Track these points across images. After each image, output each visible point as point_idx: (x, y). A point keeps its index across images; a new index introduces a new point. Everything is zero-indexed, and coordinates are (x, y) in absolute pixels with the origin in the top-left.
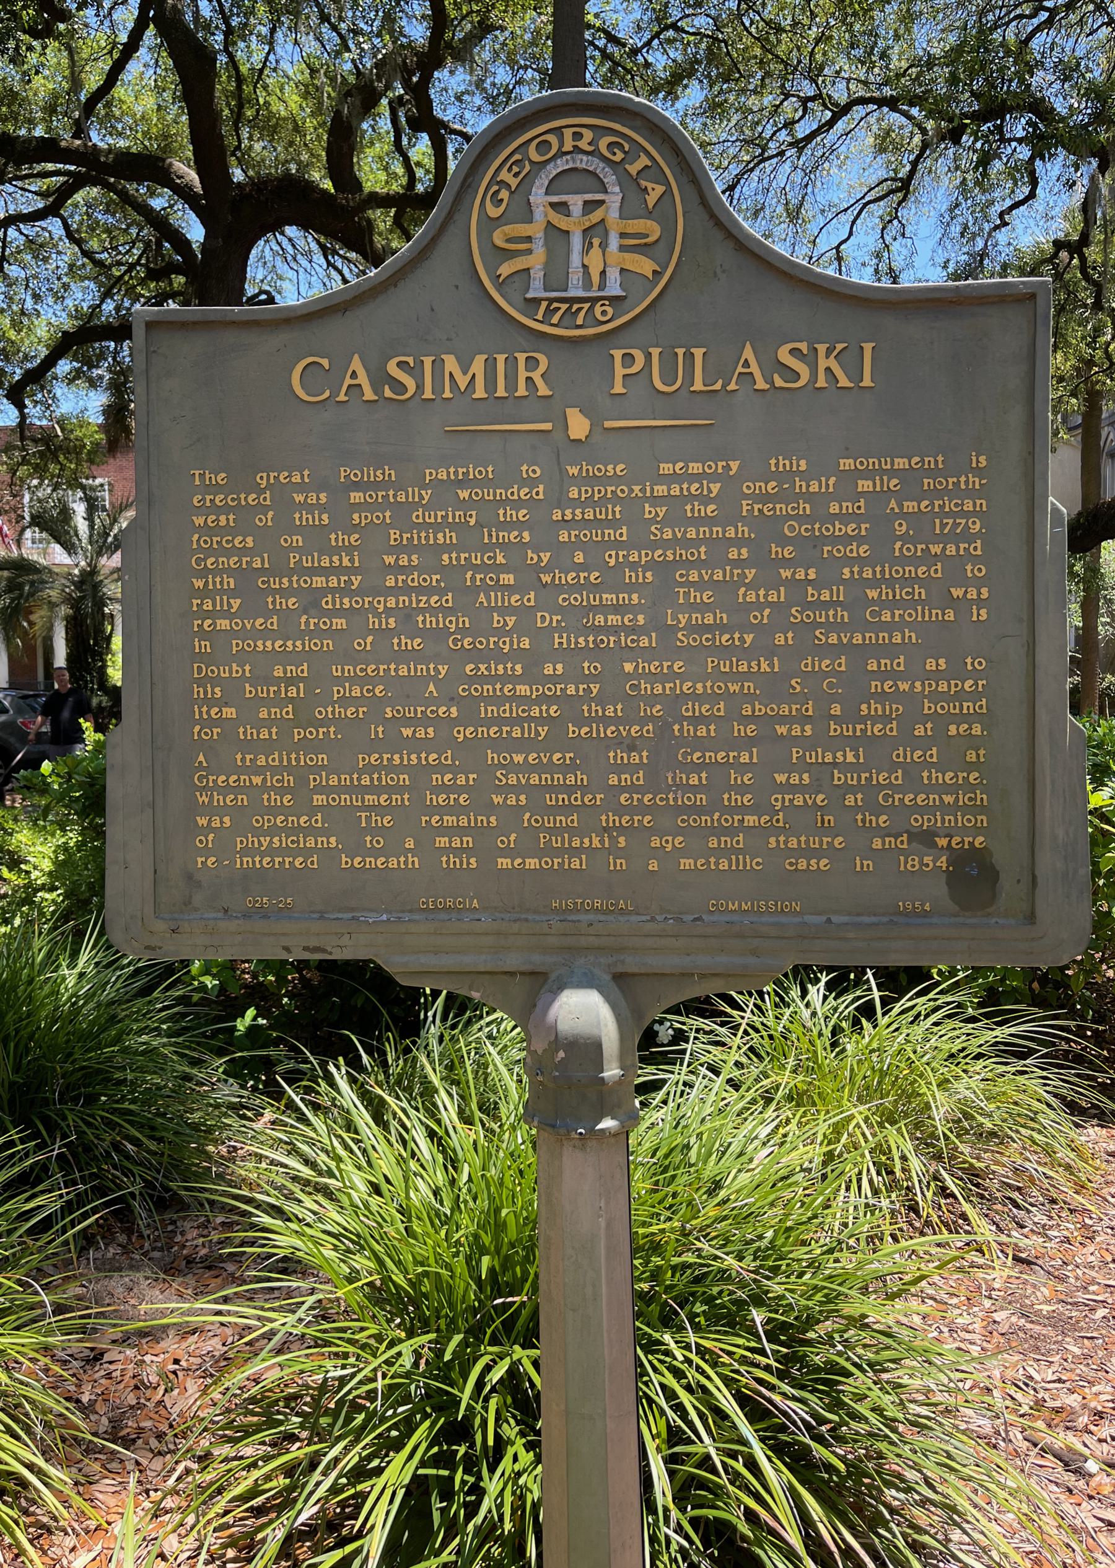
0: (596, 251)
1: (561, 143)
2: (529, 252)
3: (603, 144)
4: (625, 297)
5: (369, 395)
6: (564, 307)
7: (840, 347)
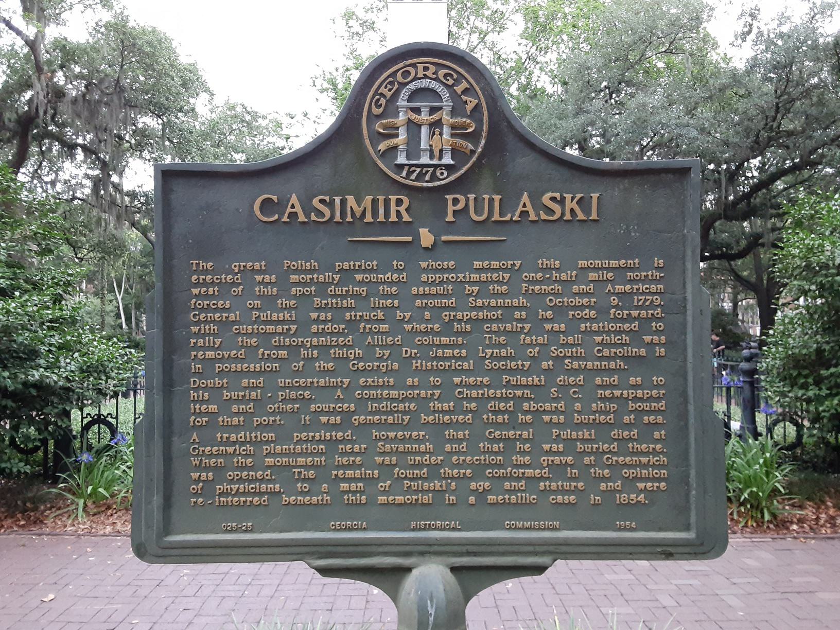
3: (442, 72)
5: (302, 218)
6: (418, 170)
7: (579, 196)
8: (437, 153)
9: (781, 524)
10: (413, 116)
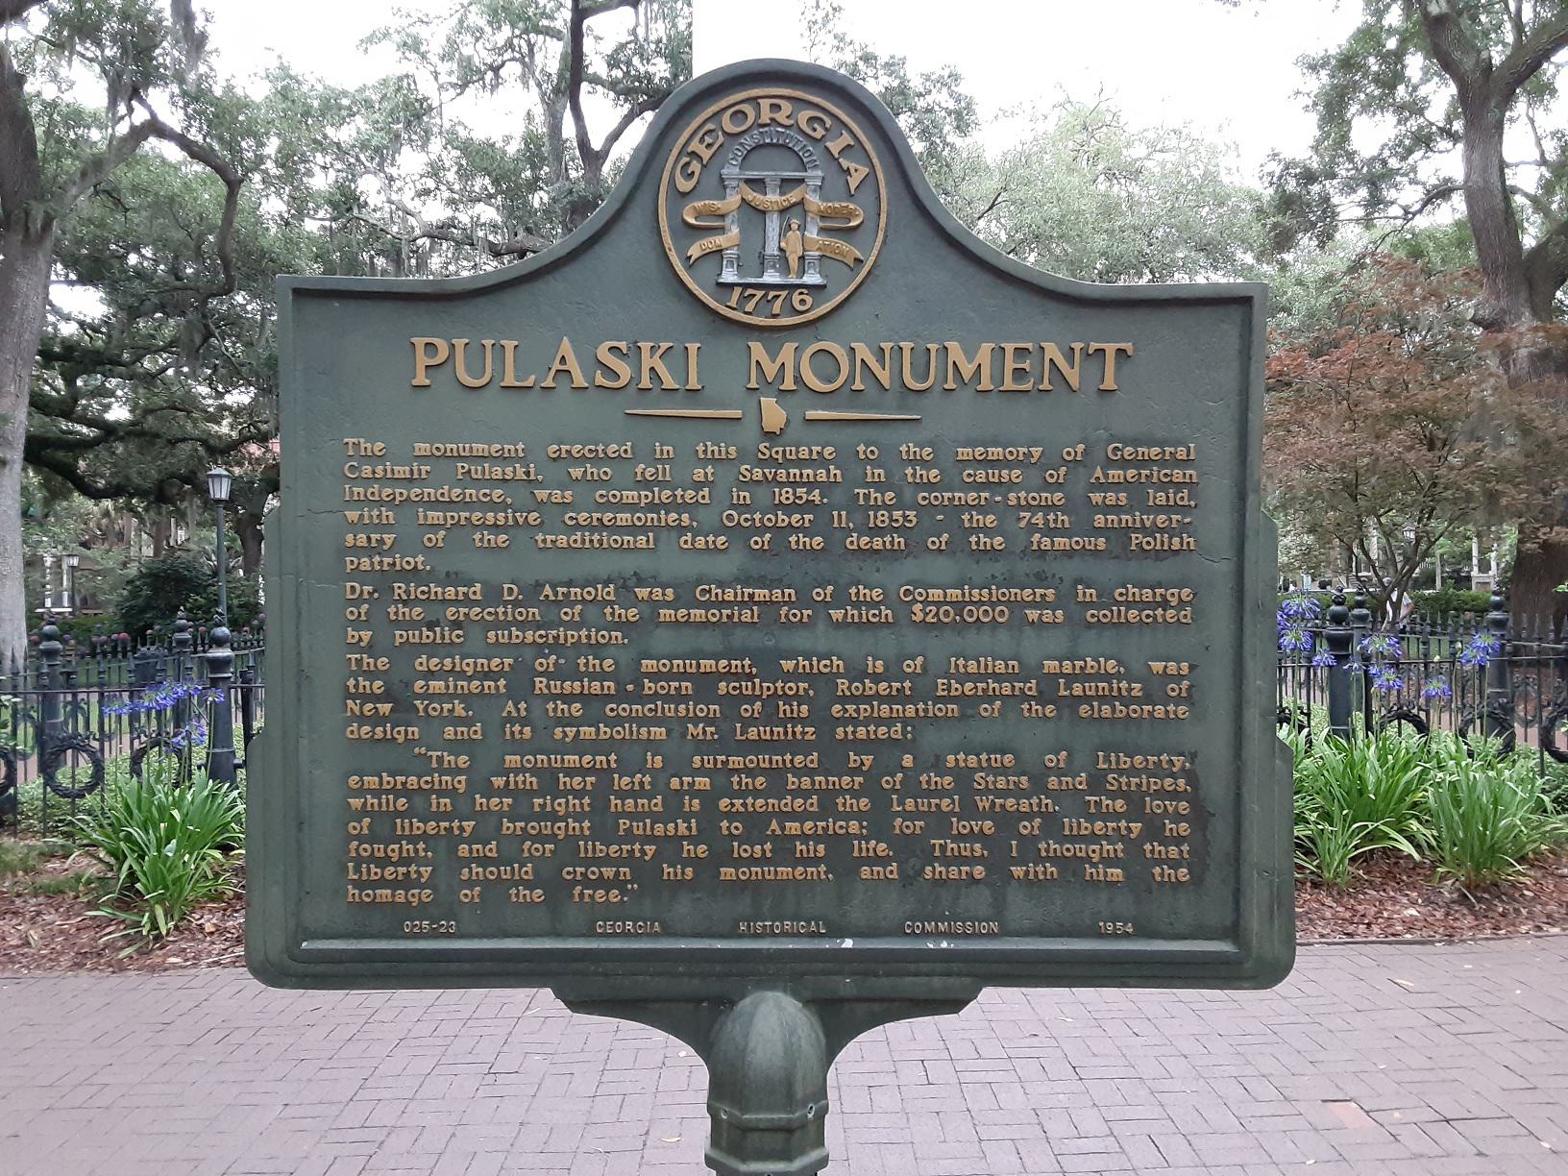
0: (794, 235)
1: (758, 115)
2: (722, 230)
3: (804, 115)
4: (824, 287)
5: (580, 380)
6: (760, 294)
7: (665, 345)
8: (794, 263)
9: (120, 968)
10: (751, 196)
